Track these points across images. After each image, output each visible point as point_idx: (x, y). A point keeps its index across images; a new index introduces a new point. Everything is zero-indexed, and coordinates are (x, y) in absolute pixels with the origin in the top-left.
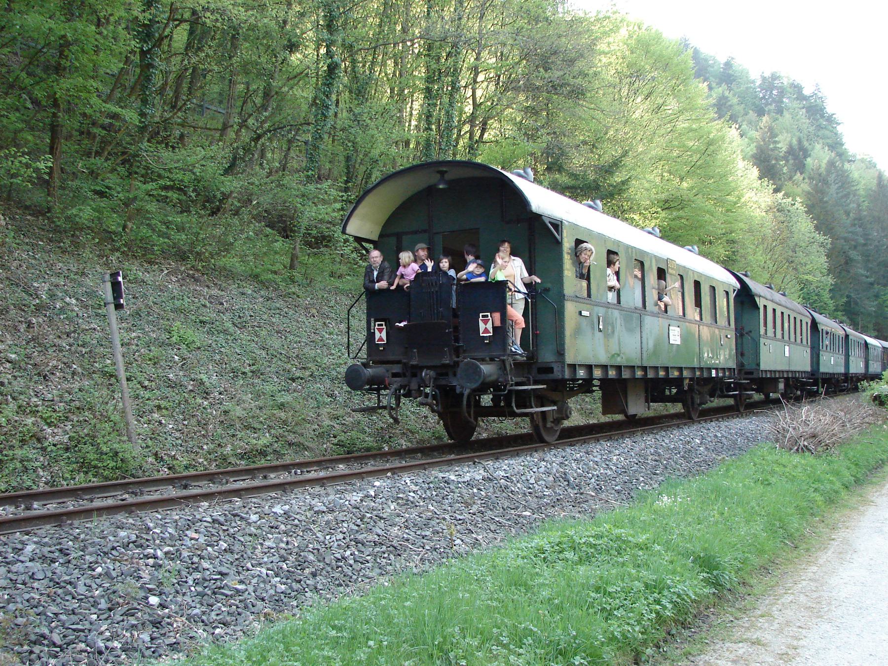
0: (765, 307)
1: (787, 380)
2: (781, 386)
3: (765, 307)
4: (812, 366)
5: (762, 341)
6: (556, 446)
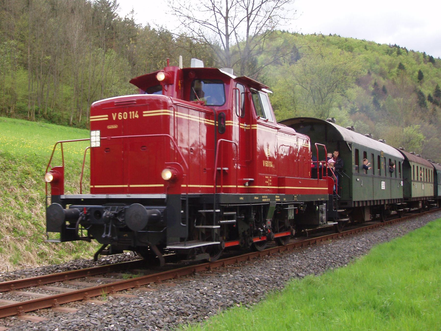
0: (414, 166)
1: (423, 201)
2: (420, 205)
3: (414, 166)
4: (434, 193)
5: (412, 183)
6: (374, 228)
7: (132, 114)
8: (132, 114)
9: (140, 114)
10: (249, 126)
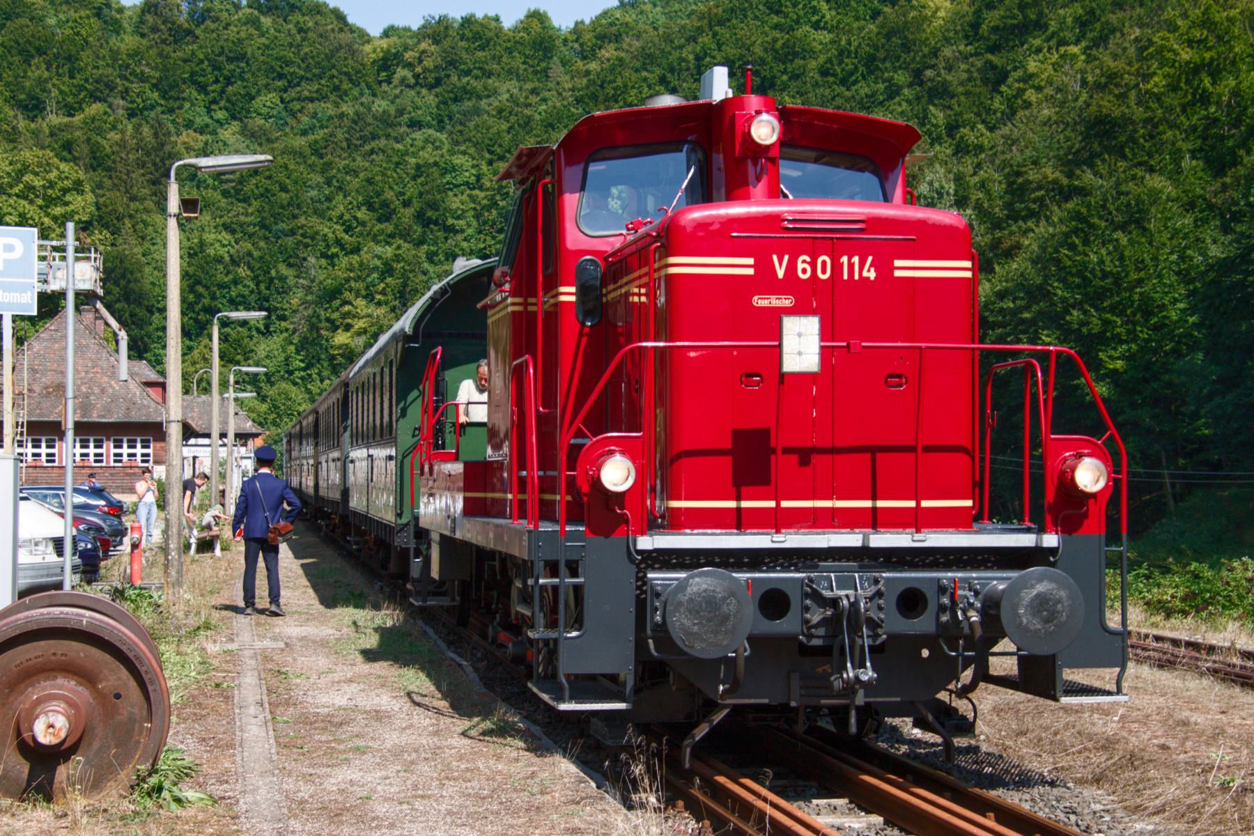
7: (851, 266)
8: (851, 266)
9: (885, 268)
10: (531, 308)
